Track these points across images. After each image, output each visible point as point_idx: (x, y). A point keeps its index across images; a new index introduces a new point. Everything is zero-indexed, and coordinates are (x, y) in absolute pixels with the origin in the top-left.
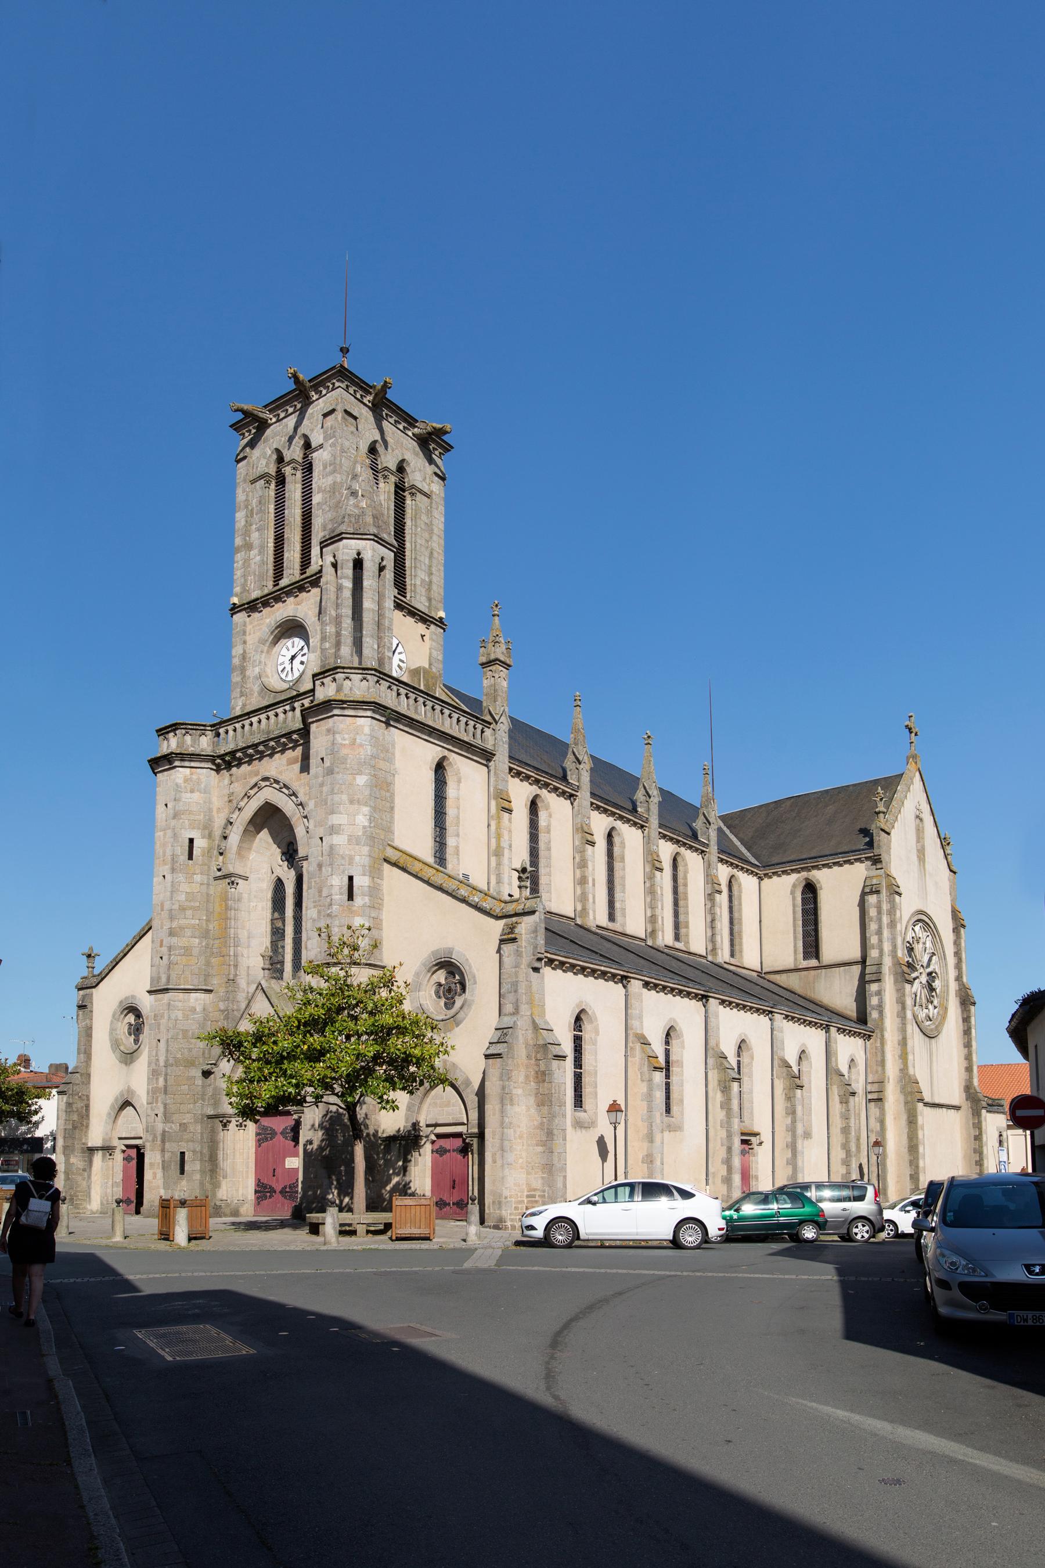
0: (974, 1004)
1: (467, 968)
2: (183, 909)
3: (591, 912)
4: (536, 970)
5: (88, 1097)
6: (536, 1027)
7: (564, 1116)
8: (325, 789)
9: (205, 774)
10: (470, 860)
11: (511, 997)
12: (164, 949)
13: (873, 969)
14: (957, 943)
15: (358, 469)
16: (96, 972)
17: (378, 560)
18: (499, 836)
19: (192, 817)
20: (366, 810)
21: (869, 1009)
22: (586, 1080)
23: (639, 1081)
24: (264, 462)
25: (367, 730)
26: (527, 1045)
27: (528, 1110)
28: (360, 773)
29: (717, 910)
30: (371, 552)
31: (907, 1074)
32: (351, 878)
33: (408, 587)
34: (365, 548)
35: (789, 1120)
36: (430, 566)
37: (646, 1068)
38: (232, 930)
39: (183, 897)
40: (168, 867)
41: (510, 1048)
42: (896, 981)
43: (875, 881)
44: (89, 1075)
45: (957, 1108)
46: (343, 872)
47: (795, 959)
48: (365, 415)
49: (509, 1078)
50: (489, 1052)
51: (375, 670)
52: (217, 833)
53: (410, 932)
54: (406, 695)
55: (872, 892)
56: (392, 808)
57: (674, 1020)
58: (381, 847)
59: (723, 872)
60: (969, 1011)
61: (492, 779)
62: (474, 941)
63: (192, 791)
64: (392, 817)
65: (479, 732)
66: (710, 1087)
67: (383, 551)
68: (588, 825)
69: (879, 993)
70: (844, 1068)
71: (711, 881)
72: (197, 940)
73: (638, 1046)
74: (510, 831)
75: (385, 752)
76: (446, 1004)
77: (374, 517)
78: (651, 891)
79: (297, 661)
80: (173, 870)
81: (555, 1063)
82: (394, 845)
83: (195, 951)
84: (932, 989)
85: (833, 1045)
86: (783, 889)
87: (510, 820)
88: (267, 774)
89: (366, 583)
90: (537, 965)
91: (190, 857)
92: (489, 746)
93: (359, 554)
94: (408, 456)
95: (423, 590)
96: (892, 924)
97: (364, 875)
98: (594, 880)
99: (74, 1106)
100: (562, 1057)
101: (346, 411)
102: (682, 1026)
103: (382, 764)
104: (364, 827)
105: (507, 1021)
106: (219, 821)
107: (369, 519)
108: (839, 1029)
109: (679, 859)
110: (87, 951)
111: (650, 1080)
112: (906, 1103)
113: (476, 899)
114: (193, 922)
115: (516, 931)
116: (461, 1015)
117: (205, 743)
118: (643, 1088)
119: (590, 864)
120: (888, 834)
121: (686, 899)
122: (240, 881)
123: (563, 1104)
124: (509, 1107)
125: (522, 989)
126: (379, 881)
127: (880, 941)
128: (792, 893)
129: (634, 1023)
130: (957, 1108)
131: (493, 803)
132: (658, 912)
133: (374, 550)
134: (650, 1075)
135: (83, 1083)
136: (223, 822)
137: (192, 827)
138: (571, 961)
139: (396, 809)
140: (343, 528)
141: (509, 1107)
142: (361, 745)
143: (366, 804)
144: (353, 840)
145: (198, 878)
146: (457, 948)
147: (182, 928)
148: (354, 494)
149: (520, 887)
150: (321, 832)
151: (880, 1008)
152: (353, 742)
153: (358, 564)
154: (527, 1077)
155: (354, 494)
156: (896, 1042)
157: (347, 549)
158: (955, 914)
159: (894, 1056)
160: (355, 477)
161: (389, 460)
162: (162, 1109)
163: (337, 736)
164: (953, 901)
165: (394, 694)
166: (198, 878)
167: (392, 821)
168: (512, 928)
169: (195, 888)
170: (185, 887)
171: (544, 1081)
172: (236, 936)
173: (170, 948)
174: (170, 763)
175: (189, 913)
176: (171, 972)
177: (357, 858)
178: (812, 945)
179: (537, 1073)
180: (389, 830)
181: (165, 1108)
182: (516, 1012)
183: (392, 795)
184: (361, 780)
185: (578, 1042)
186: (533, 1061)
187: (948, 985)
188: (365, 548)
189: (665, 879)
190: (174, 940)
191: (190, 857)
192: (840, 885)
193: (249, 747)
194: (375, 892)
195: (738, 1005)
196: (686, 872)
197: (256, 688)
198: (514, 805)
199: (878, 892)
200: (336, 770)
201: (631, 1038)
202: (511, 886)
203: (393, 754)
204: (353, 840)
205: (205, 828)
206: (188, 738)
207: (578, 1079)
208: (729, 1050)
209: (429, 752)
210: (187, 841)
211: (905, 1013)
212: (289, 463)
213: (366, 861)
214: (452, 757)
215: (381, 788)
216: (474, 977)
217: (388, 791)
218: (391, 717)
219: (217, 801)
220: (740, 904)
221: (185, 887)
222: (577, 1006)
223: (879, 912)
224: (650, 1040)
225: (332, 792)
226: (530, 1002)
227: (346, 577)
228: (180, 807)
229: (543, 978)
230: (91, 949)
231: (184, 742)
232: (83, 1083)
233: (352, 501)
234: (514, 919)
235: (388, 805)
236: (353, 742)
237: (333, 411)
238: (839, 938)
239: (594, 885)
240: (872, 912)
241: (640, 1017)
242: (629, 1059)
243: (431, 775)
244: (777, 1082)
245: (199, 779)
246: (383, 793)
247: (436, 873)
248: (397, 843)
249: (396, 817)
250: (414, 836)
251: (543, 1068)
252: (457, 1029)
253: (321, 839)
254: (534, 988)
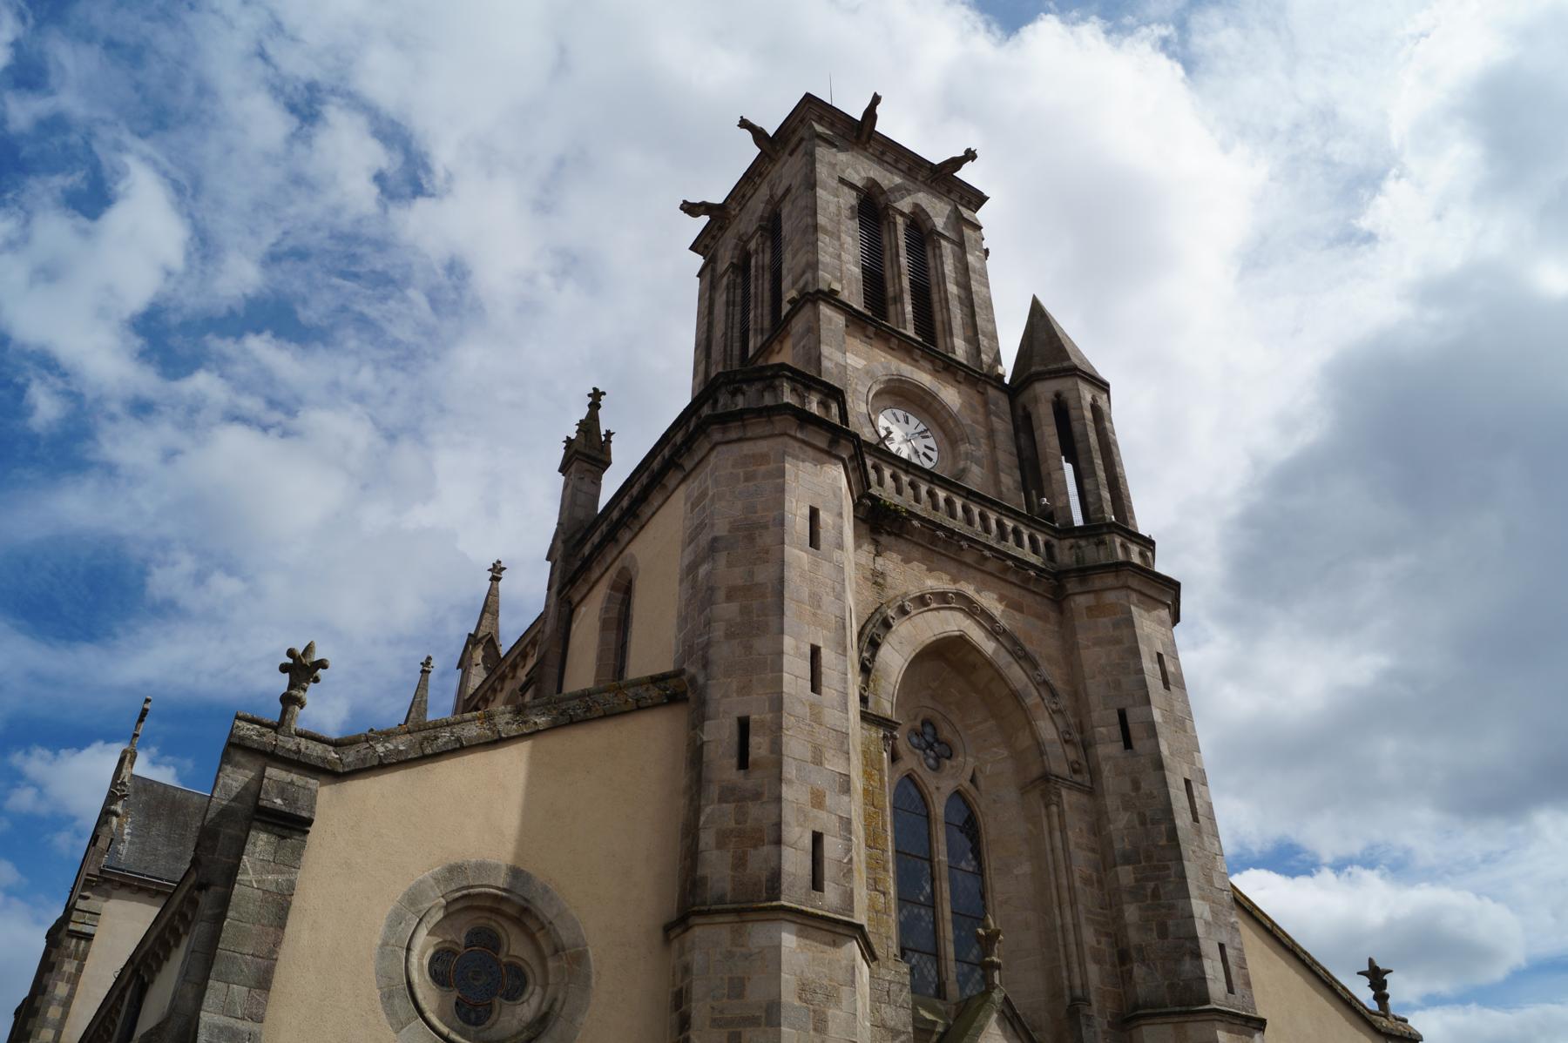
174: (834, 442)
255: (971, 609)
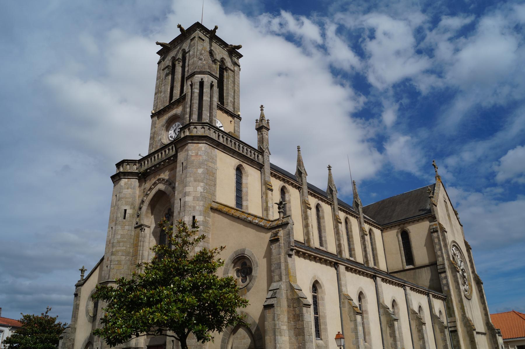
0: (482, 283)
1: (253, 258)
2: (119, 242)
3: (312, 240)
4: (290, 256)
5: (74, 339)
6: (292, 288)
7: (312, 342)
8: (183, 176)
9: (135, 182)
10: (253, 206)
11: (277, 272)
12: (109, 262)
13: (441, 267)
14: (470, 256)
15: (203, 52)
16: (84, 278)
17: (210, 82)
18: (267, 203)
19: (127, 200)
20: (202, 184)
21: (442, 286)
22: (321, 321)
23: (349, 321)
24: (168, 62)
25: (203, 149)
26: (288, 299)
27: (290, 339)
28: (200, 168)
29: (366, 243)
30: (207, 79)
31: (466, 317)
32: (194, 217)
33: (225, 103)
34: (204, 77)
35: (421, 343)
36: (234, 96)
37: (352, 313)
38: (141, 252)
39: (119, 237)
40: (114, 223)
41: (279, 302)
42: (452, 272)
43: (434, 227)
44: (75, 329)
45: (478, 333)
46: (190, 214)
47: (403, 265)
48: (207, 40)
49: (278, 319)
50: (266, 304)
51: (208, 123)
52: (137, 207)
53: (224, 241)
54: (222, 136)
55: (434, 232)
56: (215, 185)
57: (362, 289)
58: (209, 202)
59: (367, 227)
60: (481, 287)
61: (263, 176)
62: (255, 244)
63: (128, 189)
64: (215, 189)
65: (256, 156)
66: (383, 324)
67: (212, 79)
68: (308, 200)
69: (446, 277)
70: (438, 314)
71: (362, 230)
72: (124, 257)
73: (346, 301)
74: (272, 199)
75: (213, 160)
76: (242, 280)
77: (209, 67)
78: (337, 233)
79: (176, 132)
80: (116, 224)
81: (305, 309)
82: (216, 201)
83: (123, 263)
84: (464, 277)
85: (432, 303)
86: (393, 236)
87: (272, 195)
88: (160, 177)
89: (204, 90)
90: (291, 253)
91: (125, 218)
92: (261, 162)
93: (202, 79)
94: (225, 57)
95: (231, 105)
96: (446, 245)
97: (200, 215)
98: (312, 225)
99: (67, 344)
100: (308, 306)
101: (199, 37)
102: (366, 292)
103: (210, 164)
104: (201, 192)
105: (274, 285)
106: (138, 201)
107: (207, 67)
108: (433, 295)
109: (347, 220)
110: (81, 268)
111: (355, 320)
112: (468, 332)
113: (257, 221)
114: (123, 248)
115: (279, 234)
116: (250, 285)
117: (134, 169)
118: (352, 325)
119: (310, 218)
120: (436, 206)
121: (352, 238)
122: (146, 228)
123: (310, 335)
124: (279, 337)
125: (283, 267)
126: (208, 219)
127: (442, 253)
128: (397, 235)
129: (344, 289)
130: (478, 333)
131: (264, 187)
132: (342, 242)
133: (208, 78)
134: (355, 317)
135: (72, 332)
136: (140, 201)
137: (126, 204)
138: (308, 252)
139: (217, 186)
140: (196, 70)
141: (279, 337)
142: (200, 155)
143: (202, 182)
144: (195, 199)
145: (127, 227)
146: (247, 249)
147: (117, 251)
148: (201, 59)
149: (279, 212)
150: (180, 196)
151: (447, 285)
152: (197, 154)
153: (202, 84)
154: (288, 318)
155: (201, 59)
156: (458, 301)
157: (197, 78)
158: (466, 243)
159: (457, 308)
160: (201, 54)
161: (218, 57)
162: (100, 345)
163: (190, 152)
164: (464, 238)
165: (217, 135)
166: (127, 227)
167: (215, 191)
168: (276, 234)
169: (125, 232)
170: (120, 232)
171: (299, 320)
172: (142, 255)
173: (111, 261)
174: (119, 177)
175: (121, 244)
176: (111, 273)
177: (197, 207)
178: (409, 258)
179: (294, 315)
180: (214, 194)
181: (102, 344)
182: (281, 280)
183: (216, 178)
184: (200, 171)
185: (315, 298)
186: (292, 309)
187: (469, 274)
188: (204, 77)
189: (342, 227)
190: (113, 257)
191: (125, 218)
192: (418, 232)
193: (162, 162)
194: (205, 223)
195: (390, 281)
196: (351, 226)
197: (159, 144)
198: (273, 188)
199: (437, 231)
200: (188, 166)
201: (342, 297)
202: (274, 214)
203: (216, 160)
204: (195, 199)
205: (132, 204)
206: (128, 166)
207: (317, 320)
208: (389, 305)
209: (234, 162)
210: (124, 211)
211: (459, 287)
212: (177, 60)
213: (201, 208)
214: (244, 165)
215: (210, 175)
216: (257, 263)
217: (213, 176)
218: (217, 145)
219: (138, 192)
220: (375, 242)
221: (120, 232)
222: (313, 278)
223: (439, 240)
224: (352, 298)
225: (186, 177)
226: (288, 274)
227: (196, 88)
228: (122, 195)
229: (294, 260)
230: (83, 267)
231: (126, 168)
232: (72, 332)
233: (200, 62)
234: (277, 230)
235: (213, 183)
236: (197, 154)
237: (195, 37)
238: (421, 255)
239: (312, 227)
240: (436, 241)
241: (346, 285)
242: (342, 309)
243: (234, 172)
244: (412, 322)
245: (131, 183)
246: (211, 177)
247: (237, 215)
248: (217, 200)
249: (217, 189)
250: (226, 196)
251: (298, 312)
252: (248, 293)
253: (180, 199)
254: (290, 266)
255: (160, 181)
